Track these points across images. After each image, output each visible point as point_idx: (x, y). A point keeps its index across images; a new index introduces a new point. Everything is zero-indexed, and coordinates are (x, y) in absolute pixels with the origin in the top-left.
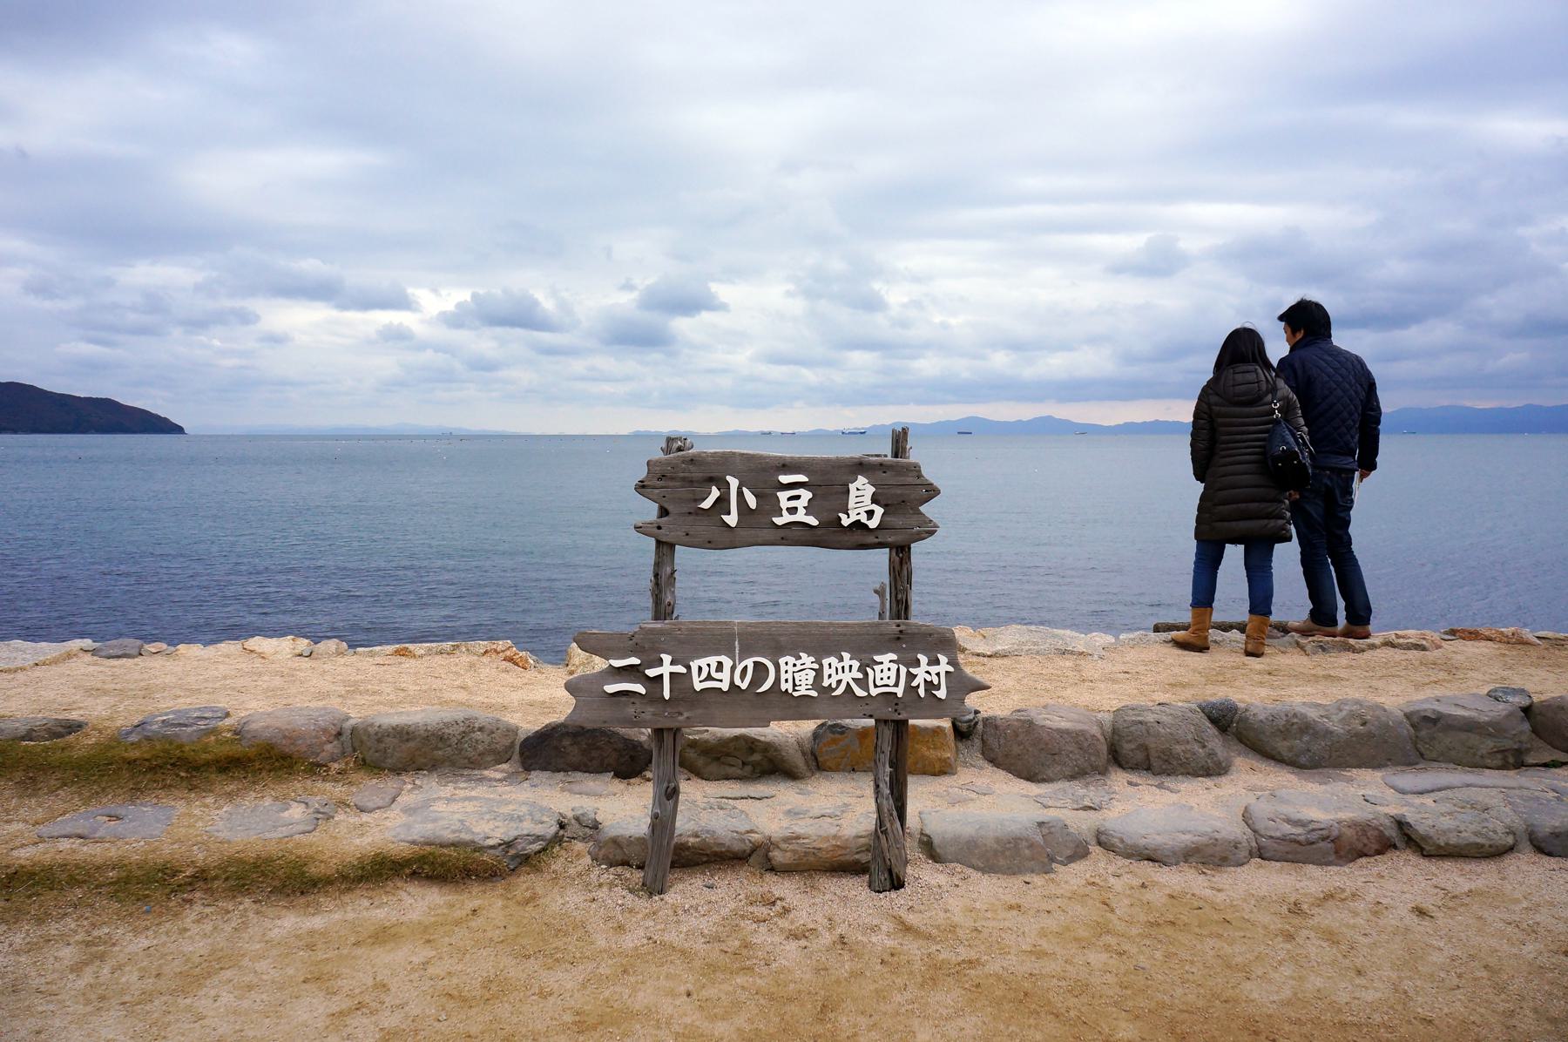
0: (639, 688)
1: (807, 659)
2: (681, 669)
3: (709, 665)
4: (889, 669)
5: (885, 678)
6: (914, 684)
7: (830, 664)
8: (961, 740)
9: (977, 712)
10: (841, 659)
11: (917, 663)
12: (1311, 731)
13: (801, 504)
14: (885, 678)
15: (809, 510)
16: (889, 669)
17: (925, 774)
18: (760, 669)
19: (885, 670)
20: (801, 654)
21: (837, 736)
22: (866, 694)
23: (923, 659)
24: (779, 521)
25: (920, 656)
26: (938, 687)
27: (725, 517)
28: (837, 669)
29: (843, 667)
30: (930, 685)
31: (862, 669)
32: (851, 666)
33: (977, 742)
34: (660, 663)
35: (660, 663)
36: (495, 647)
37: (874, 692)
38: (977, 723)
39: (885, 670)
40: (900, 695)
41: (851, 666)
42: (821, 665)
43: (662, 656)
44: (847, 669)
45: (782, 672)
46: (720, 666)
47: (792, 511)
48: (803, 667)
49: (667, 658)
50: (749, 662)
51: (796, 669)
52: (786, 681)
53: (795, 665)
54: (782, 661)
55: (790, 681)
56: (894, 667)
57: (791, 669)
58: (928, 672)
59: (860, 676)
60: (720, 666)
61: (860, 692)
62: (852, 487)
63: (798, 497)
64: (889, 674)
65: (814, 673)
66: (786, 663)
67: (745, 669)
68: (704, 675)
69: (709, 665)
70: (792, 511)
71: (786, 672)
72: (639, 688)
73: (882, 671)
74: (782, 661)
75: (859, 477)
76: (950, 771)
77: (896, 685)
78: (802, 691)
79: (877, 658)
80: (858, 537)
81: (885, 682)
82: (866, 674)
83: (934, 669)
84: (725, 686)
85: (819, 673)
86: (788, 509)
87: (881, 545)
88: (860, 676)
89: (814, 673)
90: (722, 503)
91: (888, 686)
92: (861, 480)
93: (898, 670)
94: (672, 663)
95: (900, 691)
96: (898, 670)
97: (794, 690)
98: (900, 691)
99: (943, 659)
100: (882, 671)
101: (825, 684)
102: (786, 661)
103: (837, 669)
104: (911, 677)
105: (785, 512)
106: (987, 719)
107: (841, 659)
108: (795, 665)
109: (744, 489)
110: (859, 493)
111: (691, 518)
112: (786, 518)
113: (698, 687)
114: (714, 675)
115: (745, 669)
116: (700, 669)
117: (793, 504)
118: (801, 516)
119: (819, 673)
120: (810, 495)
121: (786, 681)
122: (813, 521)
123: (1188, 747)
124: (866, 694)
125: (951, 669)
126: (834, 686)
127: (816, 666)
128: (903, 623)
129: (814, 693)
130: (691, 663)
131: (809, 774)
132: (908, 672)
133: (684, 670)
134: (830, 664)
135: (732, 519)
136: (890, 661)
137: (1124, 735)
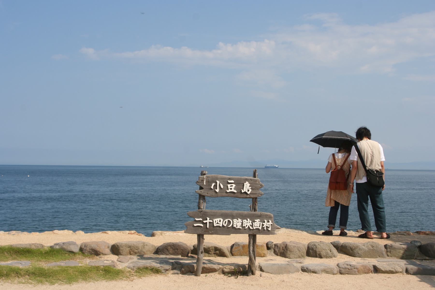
0: (202, 225)
1: (240, 220)
2: (211, 221)
3: (218, 220)
4: (258, 223)
5: (257, 225)
6: (264, 227)
7: (245, 221)
8: (268, 250)
9: (272, 243)
10: (247, 220)
11: (264, 222)
12: (358, 248)
13: (233, 187)
14: (257, 225)
15: (235, 189)
16: (258, 223)
17: (259, 257)
18: (229, 222)
19: (257, 223)
20: (238, 219)
21: (237, 247)
22: (253, 228)
23: (266, 221)
24: (228, 191)
25: (265, 220)
26: (269, 228)
27: (216, 190)
28: (246, 222)
29: (248, 222)
30: (267, 227)
31: (252, 223)
32: (249, 222)
33: (273, 250)
34: (207, 219)
35: (207, 219)
36: (131, 232)
37: (254, 228)
38: (272, 245)
39: (257, 223)
40: (260, 229)
41: (249, 222)
42: (243, 221)
43: (207, 218)
44: (249, 222)
45: (234, 223)
46: (220, 221)
47: (231, 189)
48: (239, 222)
49: (208, 219)
50: (227, 220)
51: (237, 222)
52: (235, 225)
53: (237, 221)
54: (234, 220)
55: (236, 225)
56: (259, 222)
57: (236, 222)
58: (267, 224)
59: (251, 224)
60: (220, 221)
61: (251, 228)
62: (245, 184)
63: (232, 186)
64: (258, 224)
65: (241, 223)
66: (235, 221)
67: (226, 221)
68: (216, 223)
69: (218, 220)
70: (231, 189)
71: (235, 223)
72: (202, 225)
73: (256, 223)
74: (234, 220)
75: (247, 182)
76: (266, 256)
77: (260, 227)
78: (238, 227)
79: (255, 220)
80: (245, 196)
81: (257, 226)
82: (253, 224)
83: (268, 223)
84: (221, 225)
85: (242, 223)
86: (230, 189)
87: (250, 198)
88: (251, 224)
89: (241, 223)
90: (215, 186)
91: (257, 227)
92: (247, 182)
93: (260, 223)
94: (210, 220)
95: (260, 228)
96: (260, 223)
97: (237, 227)
98: (260, 228)
99: (270, 221)
100: (256, 223)
101: (244, 226)
102: (235, 220)
103: (246, 222)
104: (263, 225)
105: (229, 189)
106: (275, 244)
107: (247, 220)
108: (237, 221)
109: (220, 184)
110: (246, 185)
111: (208, 190)
112: (229, 191)
113: (215, 225)
114: (219, 223)
115: (226, 221)
116: (216, 221)
117: (231, 187)
118: (233, 190)
119: (242, 223)
120: (235, 185)
121: (235, 225)
122: (235, 191)
123: (326, 251)
124: (253, 228)
125: (272, 223)
126: (245, 226)
127: (242, 222)
128: (262, 213)
129: (241, 228)
130: (214, 220)
131: (230, 256)
132: (262, 224)
133: (212, 221)
134: (245, 221)
135: (217, 190)
136: (258, 221)
137: (310, 248)
